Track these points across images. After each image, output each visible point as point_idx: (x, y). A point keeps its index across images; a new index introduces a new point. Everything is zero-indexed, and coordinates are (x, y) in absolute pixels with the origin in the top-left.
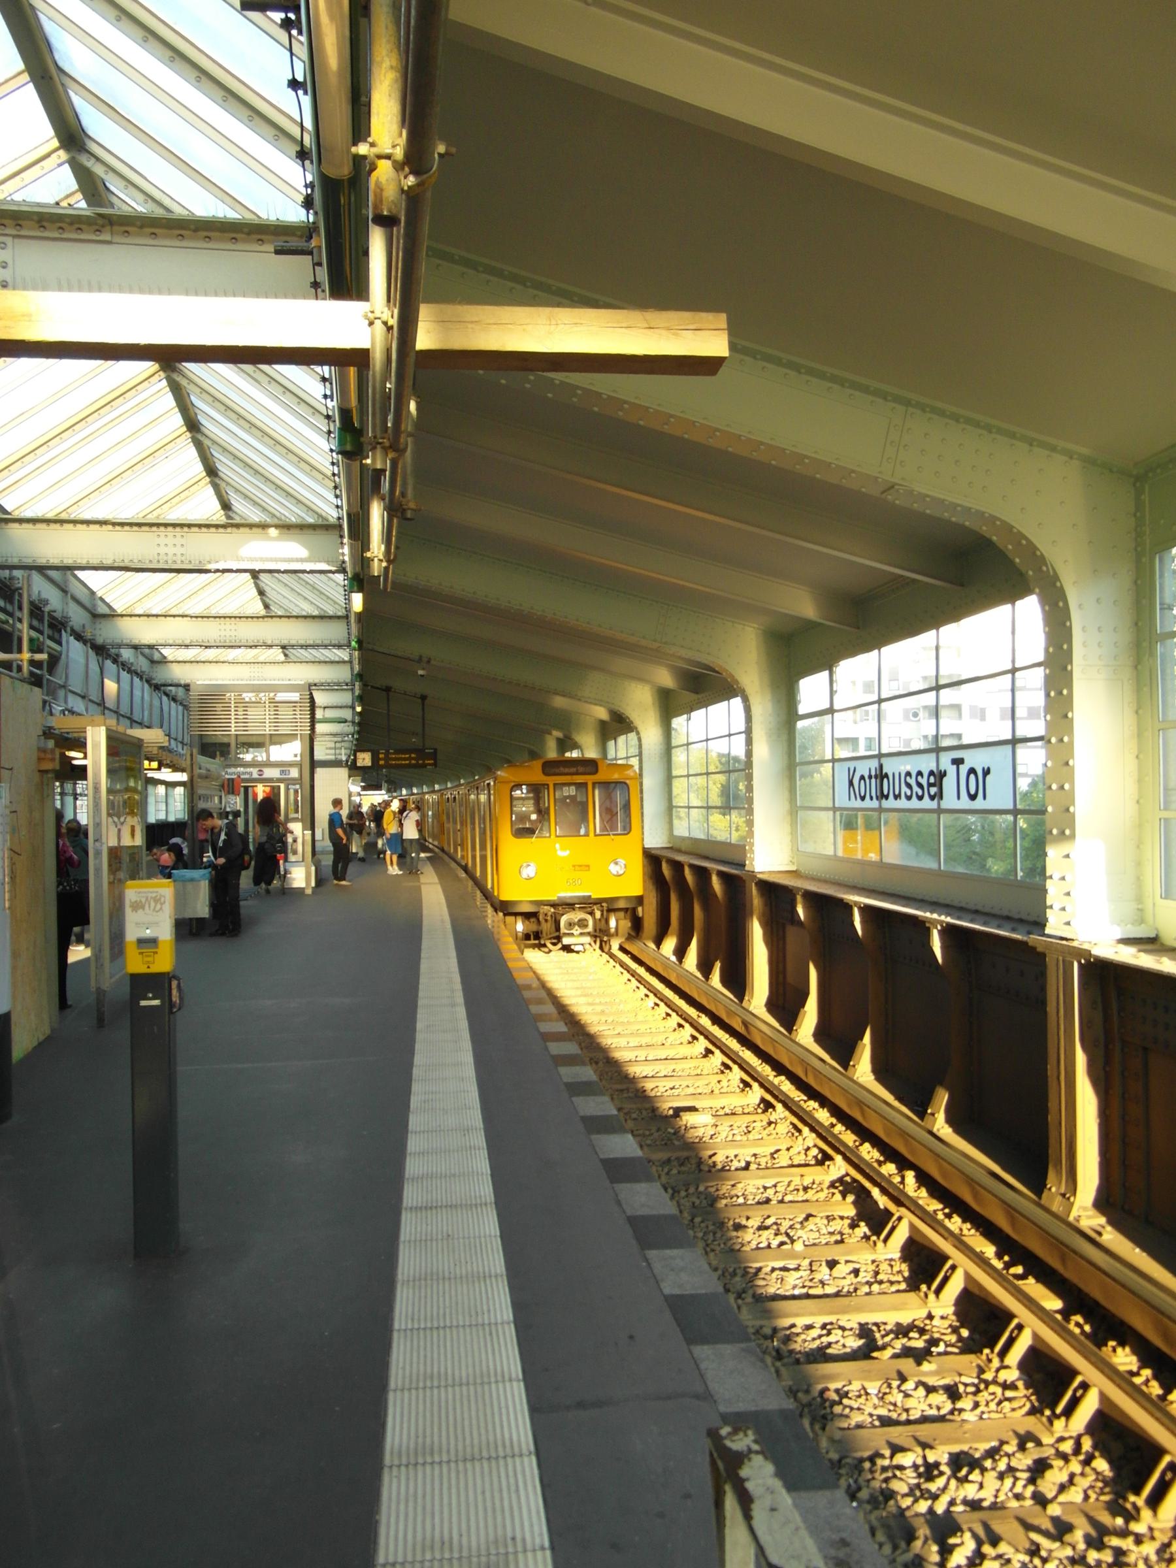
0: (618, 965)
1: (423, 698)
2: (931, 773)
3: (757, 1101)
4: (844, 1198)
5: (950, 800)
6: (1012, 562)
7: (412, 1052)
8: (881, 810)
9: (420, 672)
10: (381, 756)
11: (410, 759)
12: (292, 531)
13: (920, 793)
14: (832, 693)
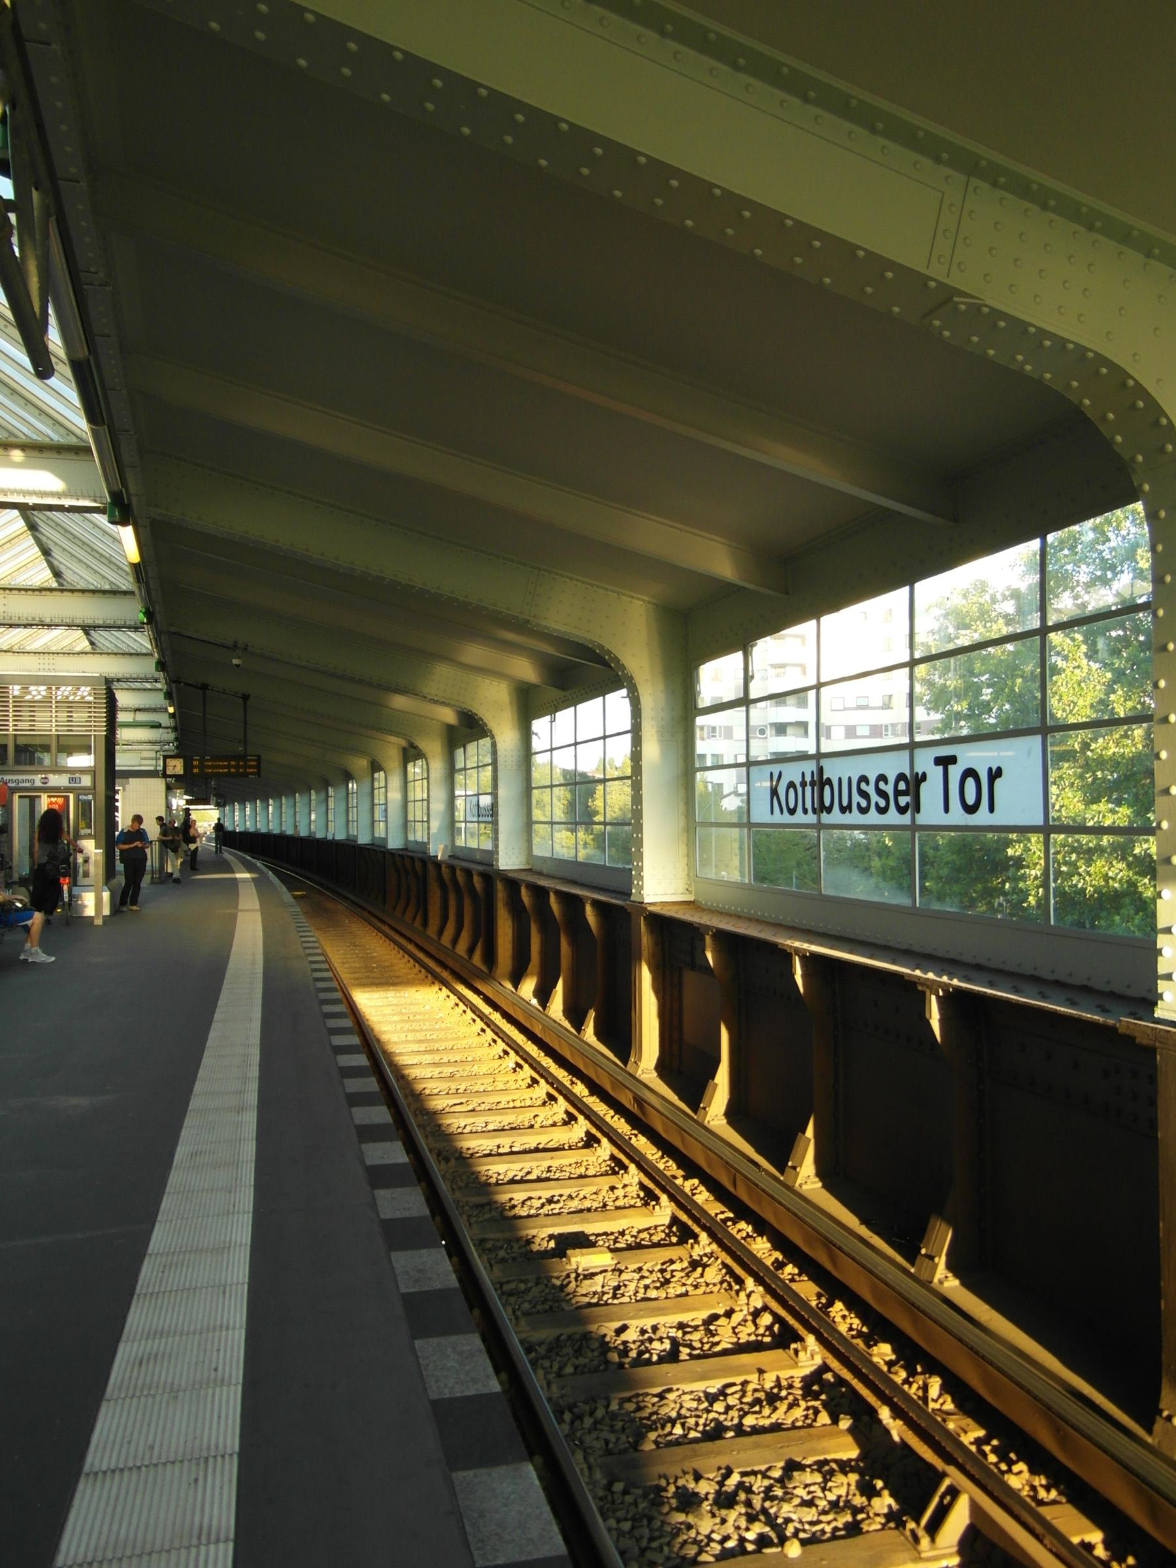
0: (468, 1011)
1: (245, 697)
2: (901, 777)
3: (667, 1221)
4: (835, 1421)
5: (931, 811)
6: (1108, 444)
7: (149, 1218)
8: (819, 826)
9: (235, 661)
10: (195, 763)
11: (228, 767)
12: (47, 454)
13: (882, 803)
14: (747, 678)
